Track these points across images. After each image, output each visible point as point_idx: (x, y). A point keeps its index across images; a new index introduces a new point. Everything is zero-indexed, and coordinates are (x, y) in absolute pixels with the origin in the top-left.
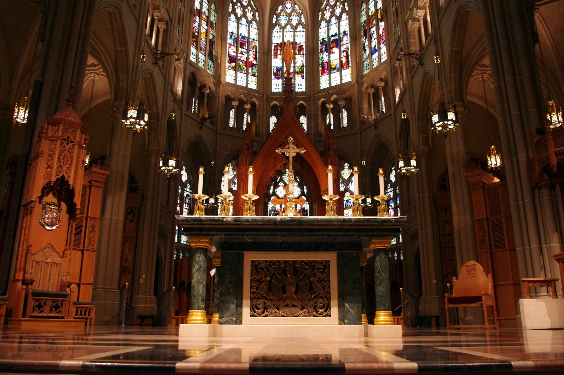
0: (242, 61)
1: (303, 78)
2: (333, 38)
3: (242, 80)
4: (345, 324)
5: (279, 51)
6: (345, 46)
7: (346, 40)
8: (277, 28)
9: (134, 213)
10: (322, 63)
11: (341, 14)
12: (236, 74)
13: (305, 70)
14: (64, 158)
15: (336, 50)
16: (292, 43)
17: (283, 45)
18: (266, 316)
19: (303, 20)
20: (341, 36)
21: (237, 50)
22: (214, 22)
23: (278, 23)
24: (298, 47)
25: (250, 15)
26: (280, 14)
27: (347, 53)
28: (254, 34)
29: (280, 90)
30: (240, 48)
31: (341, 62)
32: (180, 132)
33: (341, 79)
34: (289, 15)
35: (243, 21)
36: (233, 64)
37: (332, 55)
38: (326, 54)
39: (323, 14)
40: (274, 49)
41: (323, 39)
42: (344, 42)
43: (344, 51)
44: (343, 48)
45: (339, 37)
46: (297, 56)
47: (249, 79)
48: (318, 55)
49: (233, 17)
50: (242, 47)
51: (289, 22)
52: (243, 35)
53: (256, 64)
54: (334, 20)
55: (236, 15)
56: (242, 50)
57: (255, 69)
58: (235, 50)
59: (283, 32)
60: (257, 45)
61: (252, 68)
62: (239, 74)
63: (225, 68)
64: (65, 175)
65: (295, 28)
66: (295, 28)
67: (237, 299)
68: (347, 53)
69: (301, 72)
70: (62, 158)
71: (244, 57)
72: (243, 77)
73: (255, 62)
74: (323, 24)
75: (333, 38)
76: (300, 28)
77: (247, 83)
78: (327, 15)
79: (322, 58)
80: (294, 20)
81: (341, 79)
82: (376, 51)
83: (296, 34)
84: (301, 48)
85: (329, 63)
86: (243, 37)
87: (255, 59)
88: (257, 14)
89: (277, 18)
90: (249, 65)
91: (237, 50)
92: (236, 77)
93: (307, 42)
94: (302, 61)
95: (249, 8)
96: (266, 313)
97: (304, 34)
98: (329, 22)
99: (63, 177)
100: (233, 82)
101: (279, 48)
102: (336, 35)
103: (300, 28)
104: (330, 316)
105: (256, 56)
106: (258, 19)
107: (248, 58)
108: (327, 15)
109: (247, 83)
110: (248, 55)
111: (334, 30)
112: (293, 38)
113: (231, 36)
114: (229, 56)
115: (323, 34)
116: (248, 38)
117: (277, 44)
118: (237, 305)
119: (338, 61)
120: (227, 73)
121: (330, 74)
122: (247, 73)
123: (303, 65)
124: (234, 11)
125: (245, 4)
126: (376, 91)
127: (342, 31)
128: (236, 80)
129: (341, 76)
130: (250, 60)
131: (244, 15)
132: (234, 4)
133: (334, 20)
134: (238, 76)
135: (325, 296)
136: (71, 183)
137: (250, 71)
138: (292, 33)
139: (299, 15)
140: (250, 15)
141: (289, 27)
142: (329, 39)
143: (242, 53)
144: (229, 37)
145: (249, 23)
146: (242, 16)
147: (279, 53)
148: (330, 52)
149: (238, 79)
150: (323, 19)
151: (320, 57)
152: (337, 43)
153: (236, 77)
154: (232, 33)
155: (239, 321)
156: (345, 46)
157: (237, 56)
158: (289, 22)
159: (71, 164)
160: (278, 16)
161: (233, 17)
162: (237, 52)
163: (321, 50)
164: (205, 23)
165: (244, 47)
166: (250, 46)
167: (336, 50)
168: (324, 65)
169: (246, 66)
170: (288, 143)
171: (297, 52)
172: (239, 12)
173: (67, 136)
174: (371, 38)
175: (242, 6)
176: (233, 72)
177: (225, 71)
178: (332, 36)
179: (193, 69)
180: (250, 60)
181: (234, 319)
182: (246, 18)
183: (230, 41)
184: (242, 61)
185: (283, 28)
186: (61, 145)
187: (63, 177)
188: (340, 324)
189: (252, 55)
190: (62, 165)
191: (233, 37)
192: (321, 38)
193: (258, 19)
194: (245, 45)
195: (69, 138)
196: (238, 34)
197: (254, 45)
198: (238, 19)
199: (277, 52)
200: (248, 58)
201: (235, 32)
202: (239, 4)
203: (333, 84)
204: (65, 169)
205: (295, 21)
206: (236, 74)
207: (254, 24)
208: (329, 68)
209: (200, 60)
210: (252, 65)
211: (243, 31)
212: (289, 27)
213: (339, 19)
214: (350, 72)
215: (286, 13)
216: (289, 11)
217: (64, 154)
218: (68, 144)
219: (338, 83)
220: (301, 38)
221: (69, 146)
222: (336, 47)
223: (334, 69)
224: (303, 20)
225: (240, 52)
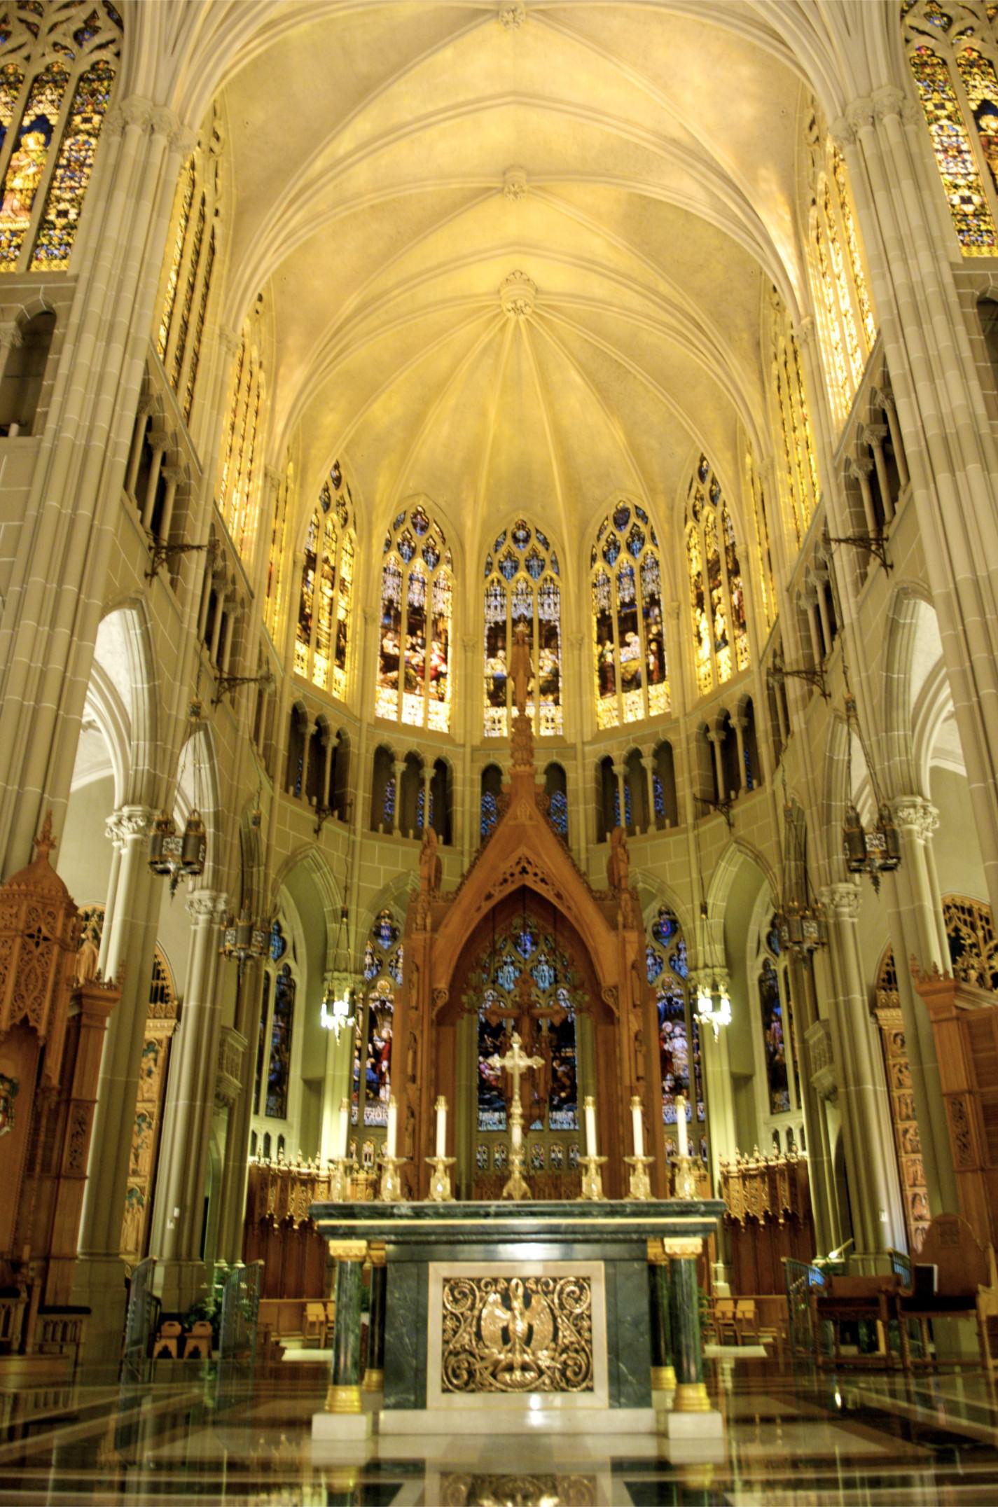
3: (413, 711)
4: (621, 1406)
9: (157, 1052)
14: (28, 976)
18: (472, 1391)
22: (348, 578)
29: (505, 733)
32: (268, 847)
47: (430, 709)
56: (414, 641)
63: (374, 685)
64: (29, 1014)
70: (23, 978)
72: (416, 705)
77: (426, 719)
81: (648, 707)
82: (726, 643)
92: (399, 705)
96: (472, 1386)
99: (25, 1020)
104: (772, 1113)
109: (426, 719)
118: (361, 720)
120: (378, 695)
126: (727, 736)
134: (404, 701)
135: (584, 1350)
136: (42, 1031)
149: (405, 710)
153: (399, 705)
155: (420, 1404)
159: (43, 989)
164: (329, 584)
170: (503, 1068)
173: (36, 927)
174: (714, 613)
177: (374, 691)
179: (298, 695)
181: (412, 1398)
186: (24, 947)
187: (25, 1020)
188: (611, 1406)
189: (438, 652)
190: (24, 993)
195: (40, 930)
204: (28, 1002)
209: (316, 671)
214: (668, 690)
217: (27, 969)
218: (37, 944)
219: (641, 715)
221: (40, 950)
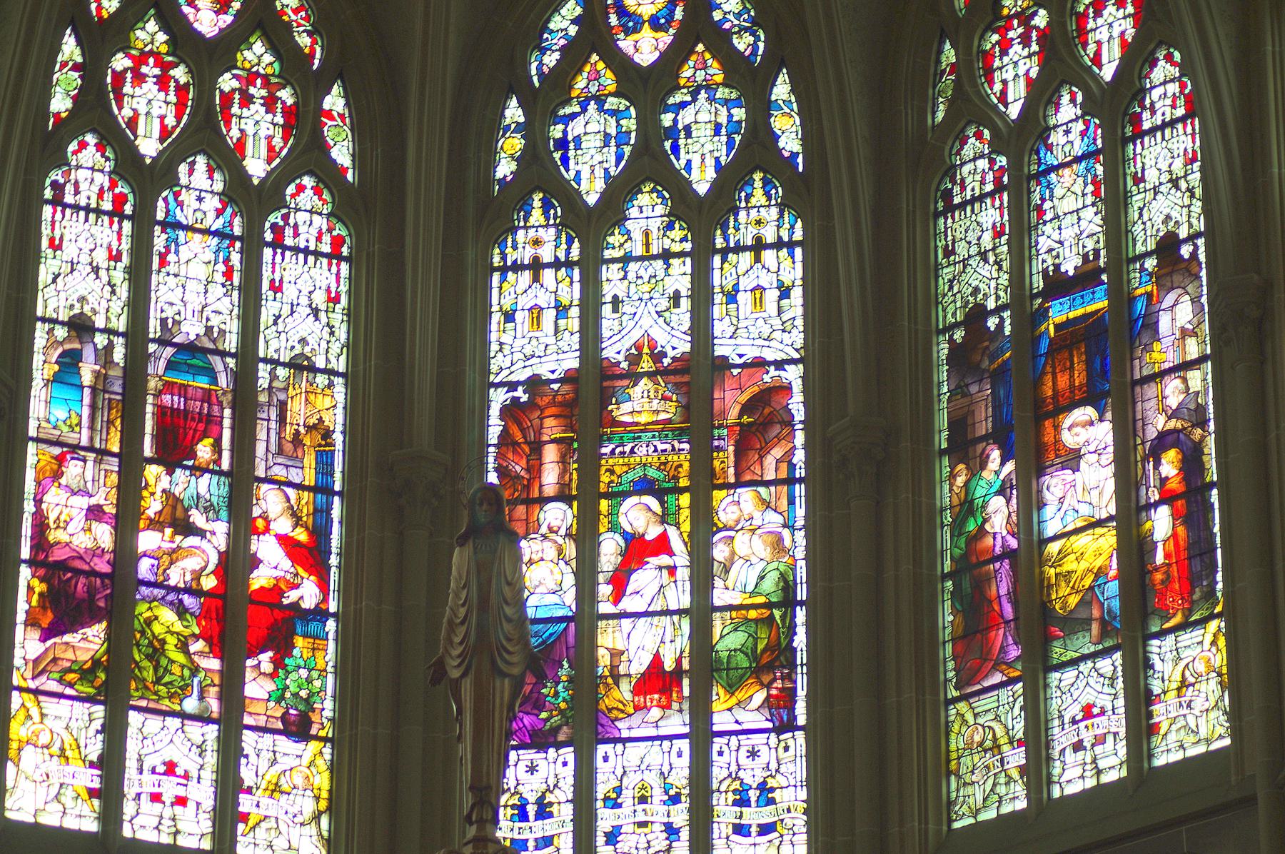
0: (174, 596)
1: (785, 726)
2: (1060, 312)
5: (550, 453)
6: (1173, 392)
7: (1180, 317)
8: (538, 235)
10: (973, 564)
11: (1137, 58)
12: (114, 732)
13: (800, 640)
15: (1088, 430)
16: (683, 366)
17: (589, 393)
19: (788, 134)
20: (1141, 286)
21: (130, 488)
23: (543, 172)
24: (731, 402)
25: (258, 131)
26: (560, 80)
27: (1192, 463)
28: (308, 306)
30: (152, 471)
31: (1134, 547)
33: (1141, 729)
34: (648, 88)
35: (199, 186)
36: (90, 641)
37: (1055, 485)
38: (998, 468)
39: (978, 67)
40: (505, 439)
41: (977, 315)
42: (1162, 354)
43: (1164, 441)
44: (1163, 405)
45: (1121, 297)
46: (727, 507)
48: (927, 485)
49: (88, 170)
50: (174, 452)
51: (650, 162)
52: (191, 330)
53: (320, 614)
54: (1069, 129)
55: (118, 140)
57: (317, 664)
58: (106, 497)
59: (590, 269)
60: (336, 420)
61: (283, 650)
62: (151, 738)
65: (704, 217)
66: (704, 217)
67: (1011, 46)
68: (1192, 463)
69: (770, 661)
71: (198, 559)
73: (308, 594)
74: (976, 165)
75: (1060, 312)
76: (760, 215)
78: (1015, 70)
79: (968, 507)
80: (703, 132)
81: (1141, 729)
83: (721, 276)
84: (764, 414)
85: (1030, 550)
86: (193, 354)
87: (309, 555)
88: (334, 101)
89: (532, 132)
90: (242, 621)
91: (130, 488)
92: (110, 764)
93: (821, 352)
94: (778, 545)
95: (257, 54)
97: (792, 269)
98: (1023, 140)
100: (84, 819)
101: (552, 428)
102: (1086, 278)
103: (760, 215)
105: (320, 532)
106: (342, 154)
107: (236, 562)
108: (1015, 70)
110: (244, 524)
111: (1070, 228)
112: (682, 316)
113: (70, 362)
114: (47, 562)
115: (973, 264)
116: (247, 354)
117: (534, 383)
119: (1107, 540)
120: (18, 730)
121: (1036, 671)
122: (230, 721)
123: (787, 586)
124: (96, 111)
125: (207, 22)
127: (1144, 239)
128: (109, 794)
129: (1140, 703)
130: (260, 579)
131: (203, 131)
132: (104, 37)
133: (1069, 129)
137: (256, 688)
138: (680, 277)
139: (749, 81)
140: (258, 131)
141: (647, 210)
142: (1029, 319)
143: (177, 520)
144: (42, 366)
145: (253, 202)
146: (179, 149)
147: (550, 477)
148: (1038, 457)
150: (973, 107)
151: (946, 495)
152: (1107, 359)
153: (110, 764)
154: (81, 326)
156: (1173, 392)
157: (125, 554)
158: (650, 162)
160: (548, 100)
161: (88, 170)
162: (126, 518)
163: (959, 425)
165: (204, 450)
166: (264, 436)
167: (1088, 430)
168: (980, 585)
169: (218, 646)
171: (725, 462)
172: (149, 110)
175: (183, 39)
176: (78, 721)
178: (1059, 285)
180: (260, 579)
182: (228, 159)
183: (49, 409)
184: (174, 596)
185: (591, 225)
191: (87, 373)
192: (952, 311)
193: (342, 154)
194: (210, 425)
196: (136, 335)
197: (298, 412)
198: (144, 182)
199: (535, 470)
200: (236, 562)
201: (110, 311)
202: (150, 34)
203: (1070, 779)
205: (701, 162)
206: (114, 732)
207: (309, 215)
208: (1025, 623)
210: (275, 626)
211: (192, 290)
212: (647, 210)
213: (1117, 111)
215: (622, 65)
216: (645, 48)
220: (765, 319)
222: (1092, 397)
223: (1073, 623)
224: (788, 134)
225: (153, 506)
